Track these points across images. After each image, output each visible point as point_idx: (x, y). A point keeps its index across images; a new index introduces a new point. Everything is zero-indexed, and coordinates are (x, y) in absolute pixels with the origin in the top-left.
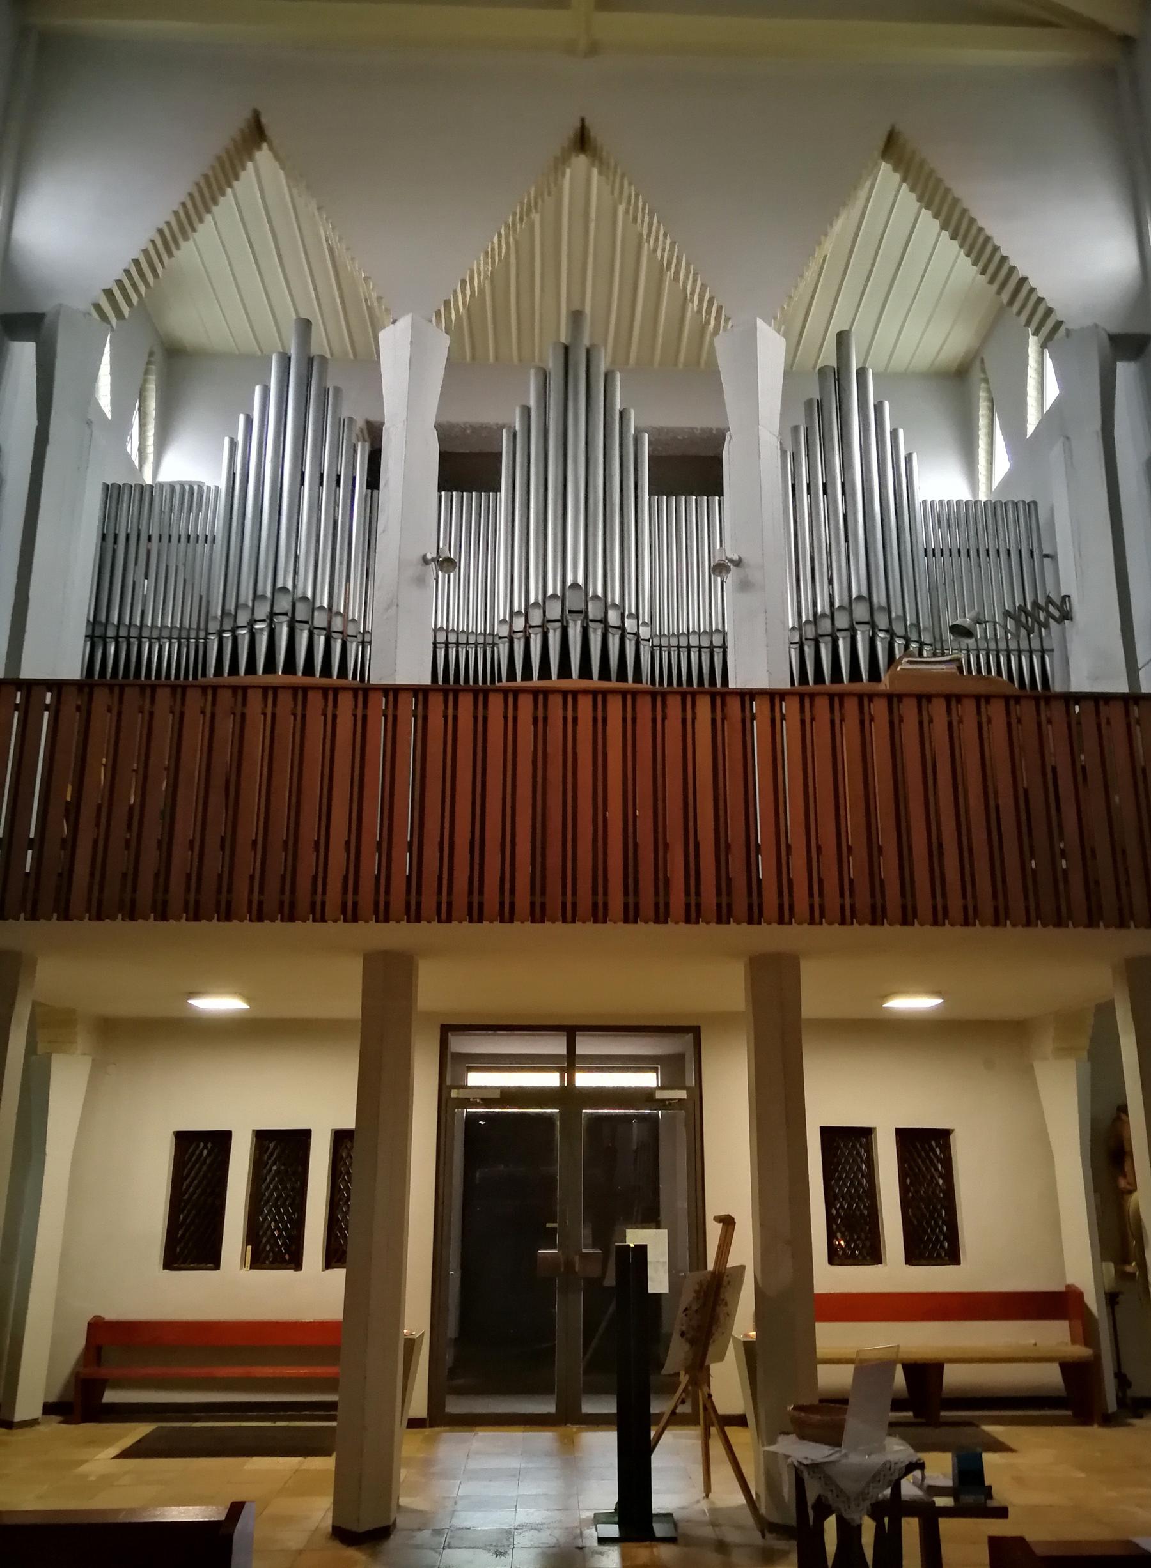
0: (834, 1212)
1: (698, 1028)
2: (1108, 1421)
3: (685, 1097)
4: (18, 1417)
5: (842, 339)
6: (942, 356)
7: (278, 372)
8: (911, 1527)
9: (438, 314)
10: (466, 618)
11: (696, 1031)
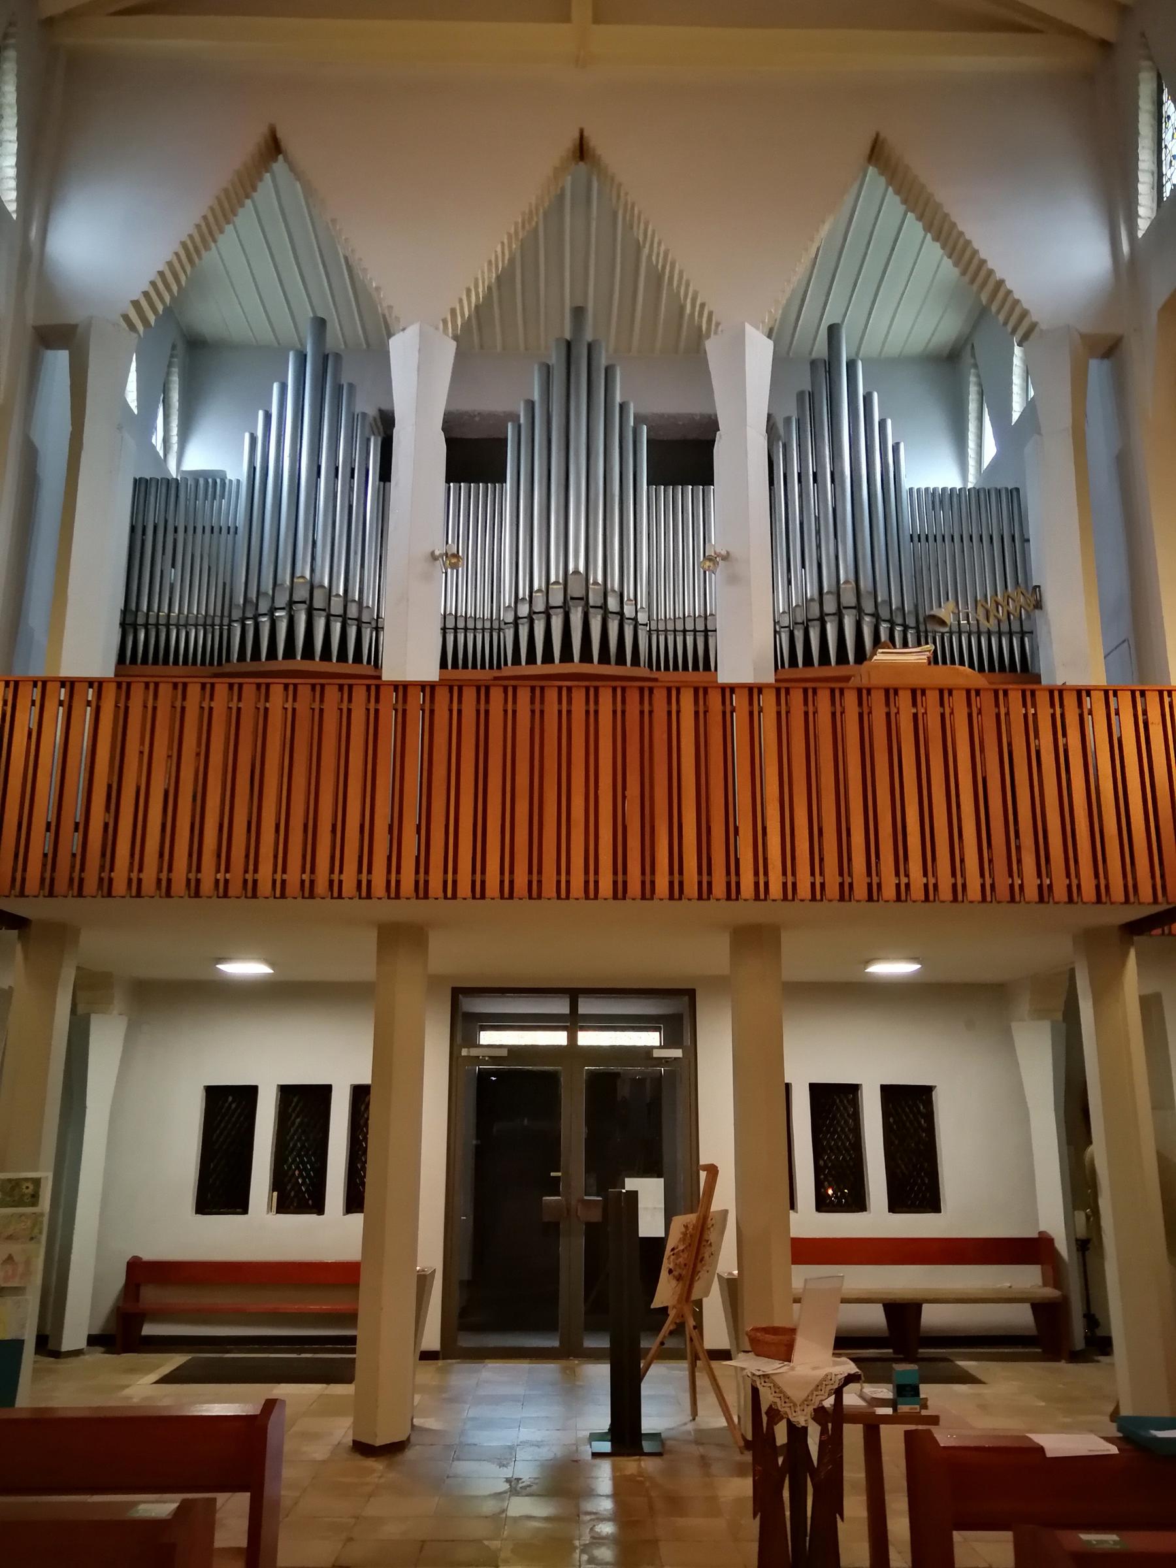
0: (821, 1163)
1: (694, 990)
2: (1075, 1357)
3: (680, 1055)
4: (66, 1346)
5: (833, 332)
6: (935, 340)
7: (295, 362)
8: (853, 1435)
9: (445, 321)
10: (472, 603)
11: (691, 994)
